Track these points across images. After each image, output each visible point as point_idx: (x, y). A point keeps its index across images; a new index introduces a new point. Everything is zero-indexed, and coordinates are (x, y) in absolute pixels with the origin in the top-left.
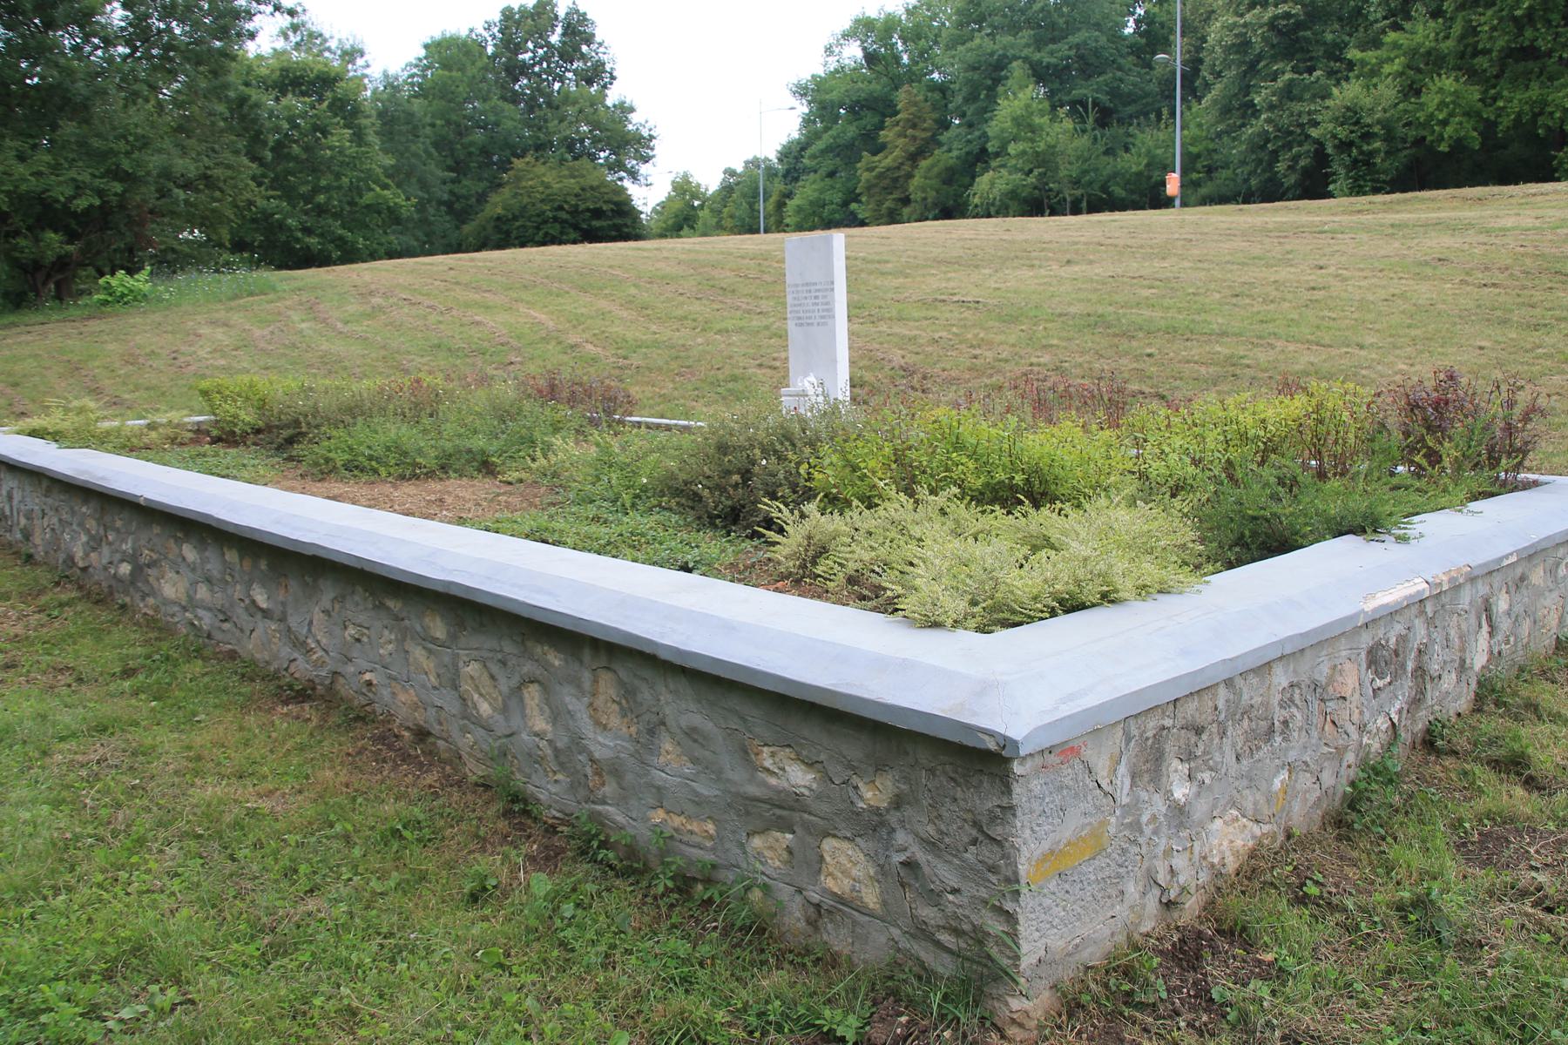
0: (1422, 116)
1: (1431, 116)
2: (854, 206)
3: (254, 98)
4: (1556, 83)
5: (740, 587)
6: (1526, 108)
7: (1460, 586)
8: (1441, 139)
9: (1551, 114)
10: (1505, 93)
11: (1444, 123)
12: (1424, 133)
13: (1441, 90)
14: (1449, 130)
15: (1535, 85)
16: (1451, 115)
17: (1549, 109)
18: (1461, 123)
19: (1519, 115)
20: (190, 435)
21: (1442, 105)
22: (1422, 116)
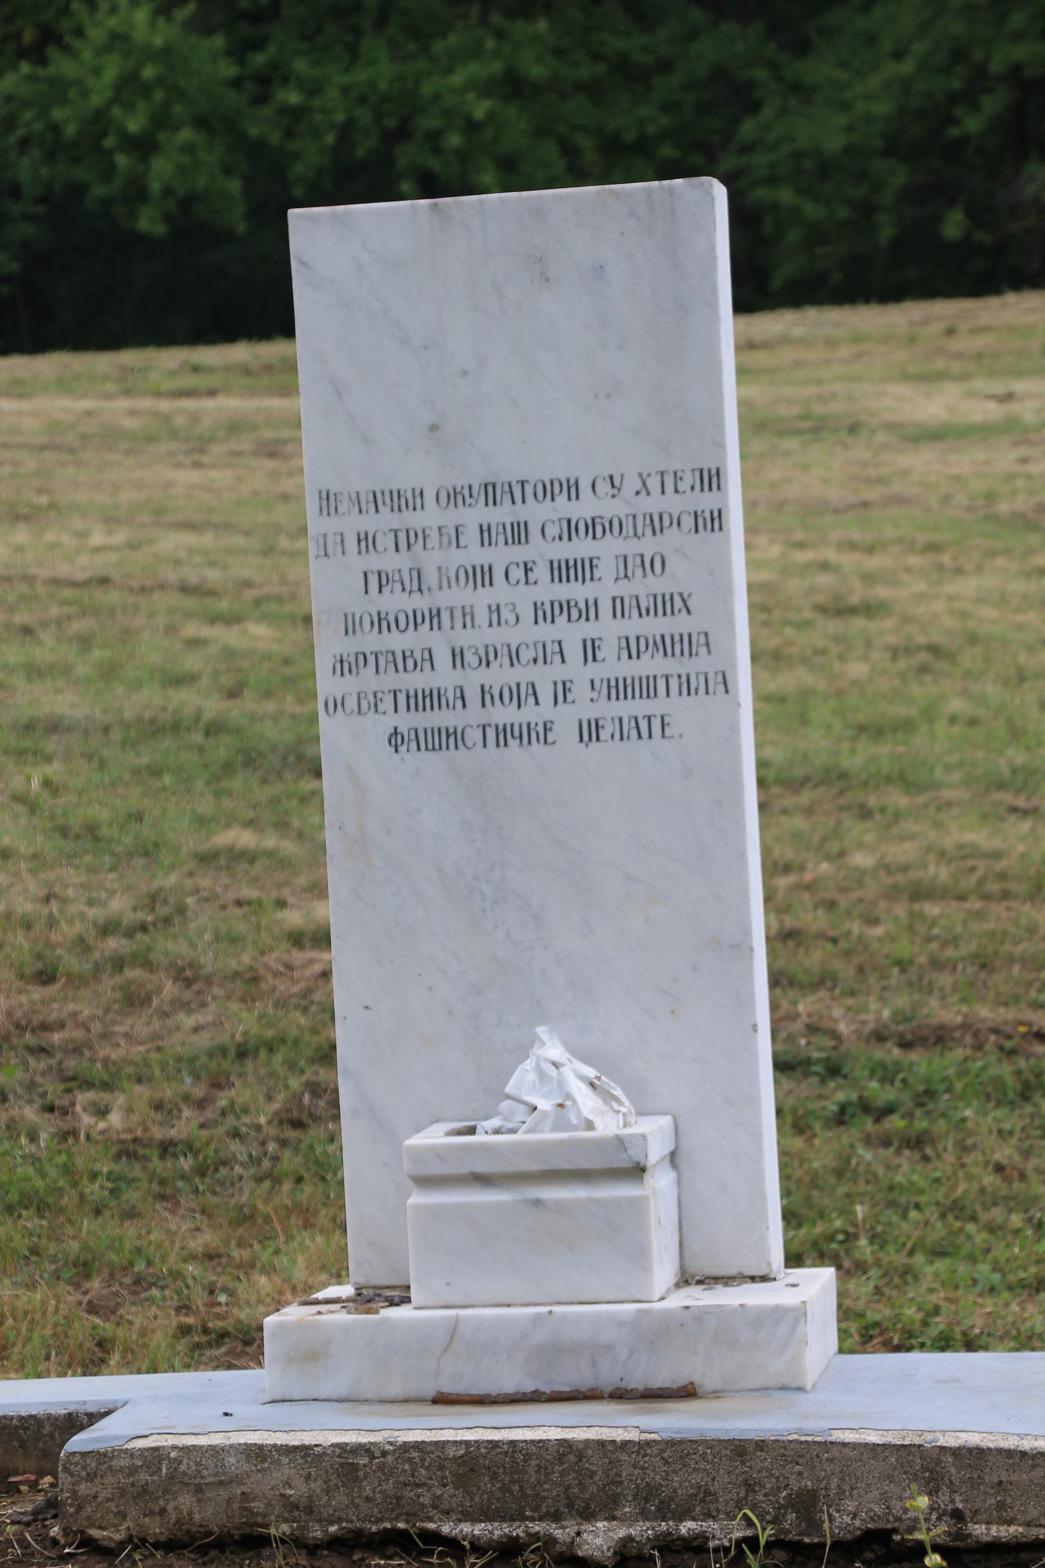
0: (67, 118)
1: (99, 119)
2: (895, 971)
3: (117, 978)
4: (438, 47)
5: (1027, 1354)
6: (364, 115)
7: (264, 1541)
8: (136, 193)
9: (434, 138)
10: (301, 66)
11: (143, 147)
12: (80, 174)
13: (117, 40)
14: (161, 169)
15: (373, 46)
16: (161, 121)
17: (428, 122)
18: (189, 149)
19: (347, 131)
20: (31, 1518)
21: (129, 87)
22: (67, 118)
